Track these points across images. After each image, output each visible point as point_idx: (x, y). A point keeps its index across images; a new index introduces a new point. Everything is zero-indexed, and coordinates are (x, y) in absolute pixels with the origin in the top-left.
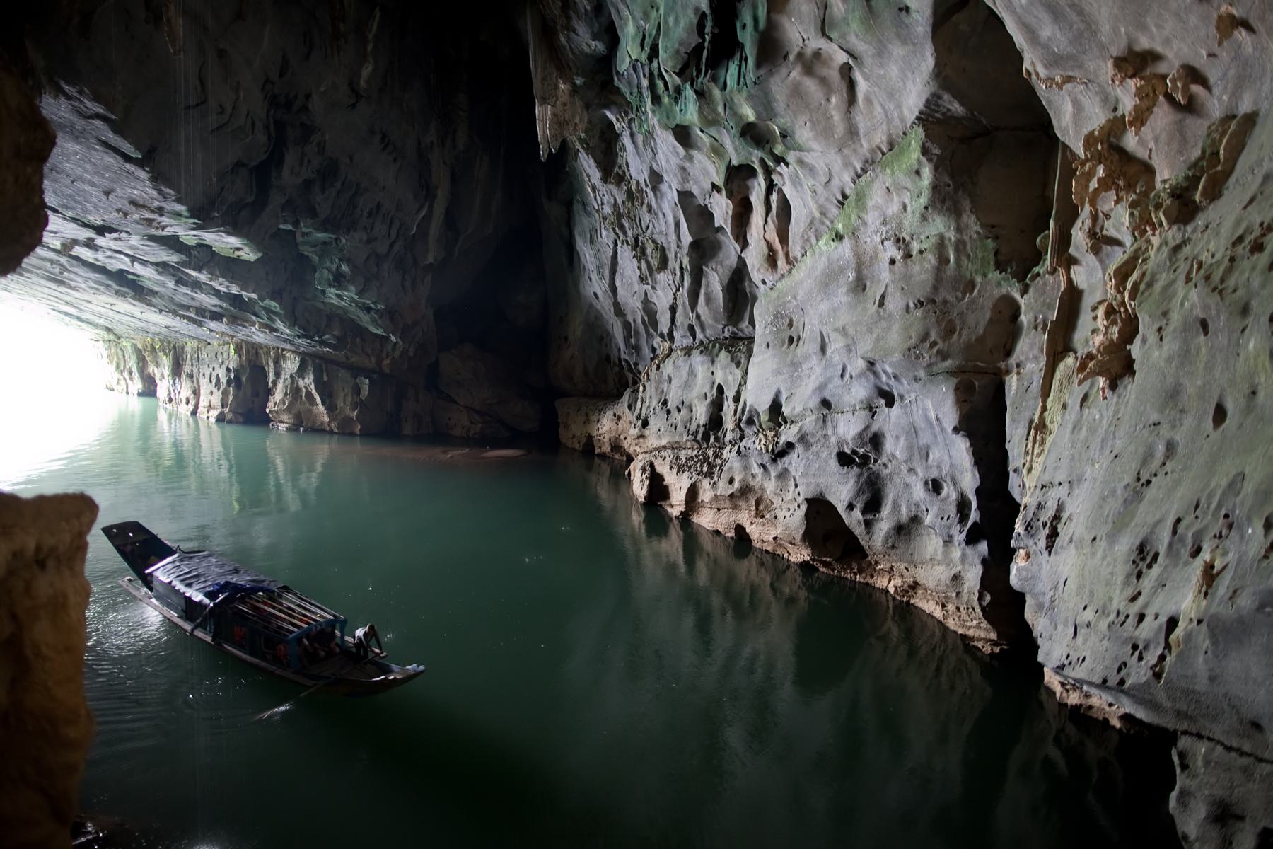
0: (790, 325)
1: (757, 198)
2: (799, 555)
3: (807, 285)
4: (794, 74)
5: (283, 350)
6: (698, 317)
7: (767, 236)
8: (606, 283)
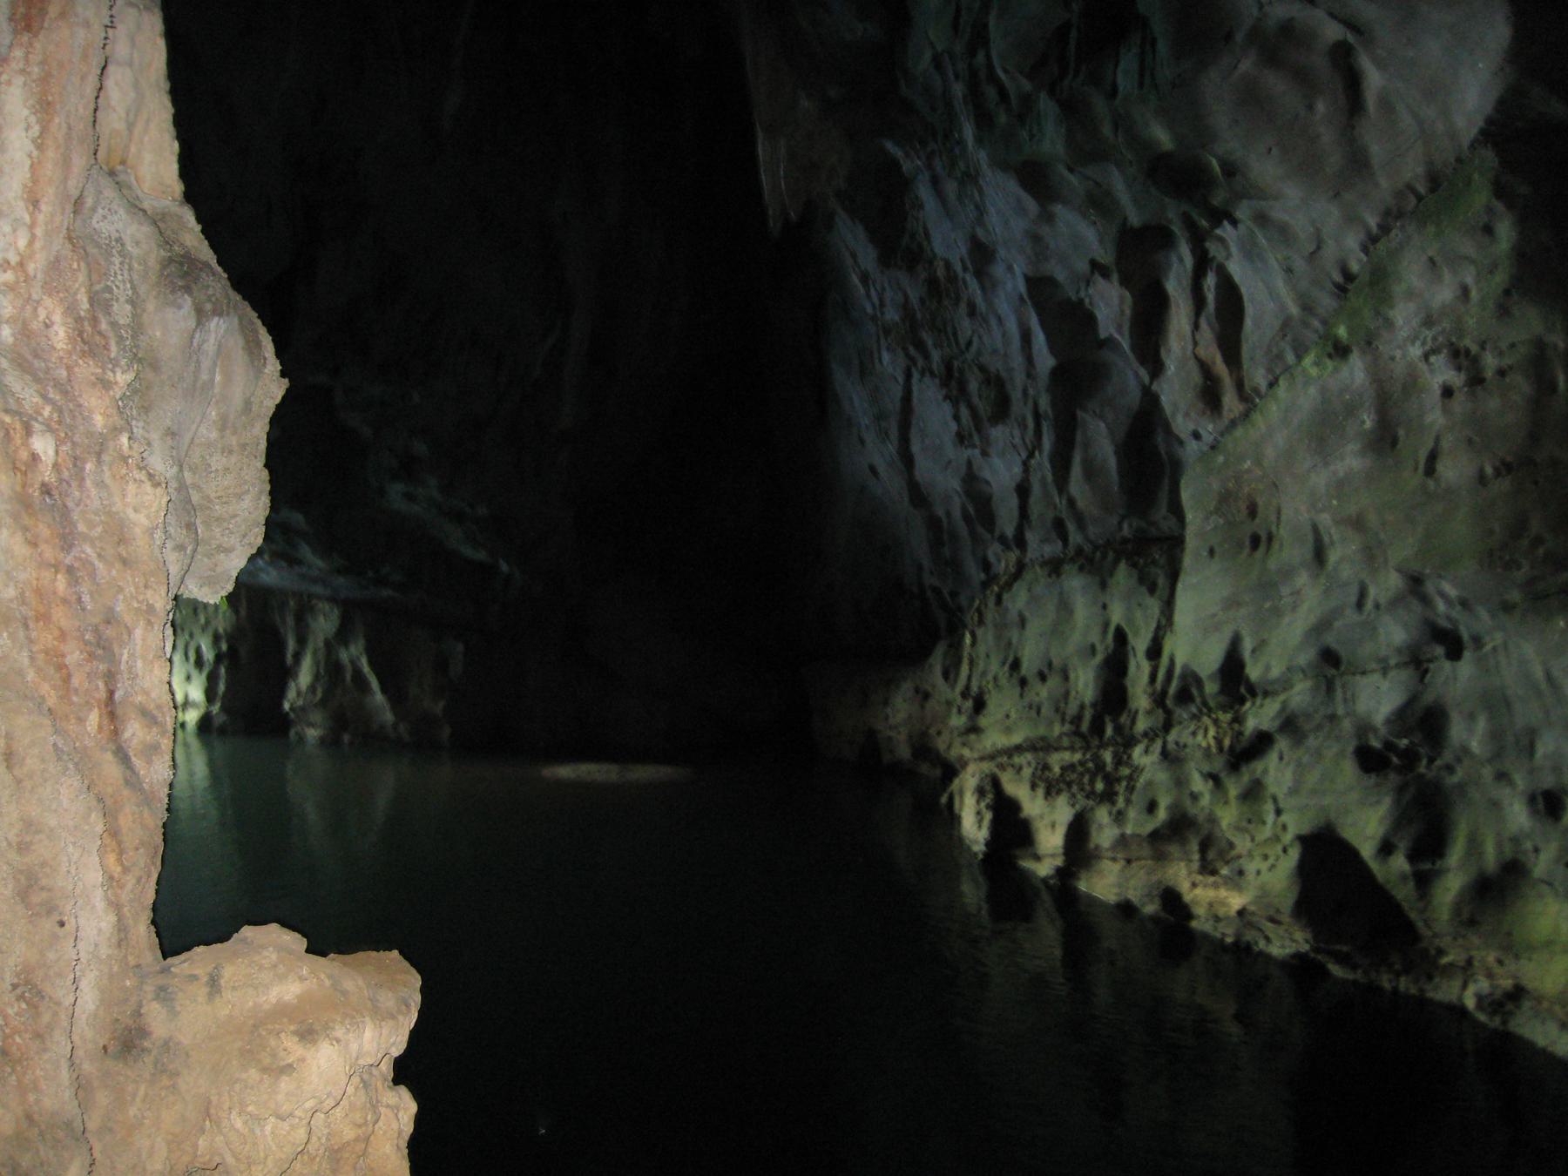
0: (1253, 511)
1: (1176, 286)
2: (1285, 942)
3: (1280, 439)
4: (1246, 65)
5: (310, 596)
6: (1071, 503)
7: (1201, 352)
8: (892, 448)
